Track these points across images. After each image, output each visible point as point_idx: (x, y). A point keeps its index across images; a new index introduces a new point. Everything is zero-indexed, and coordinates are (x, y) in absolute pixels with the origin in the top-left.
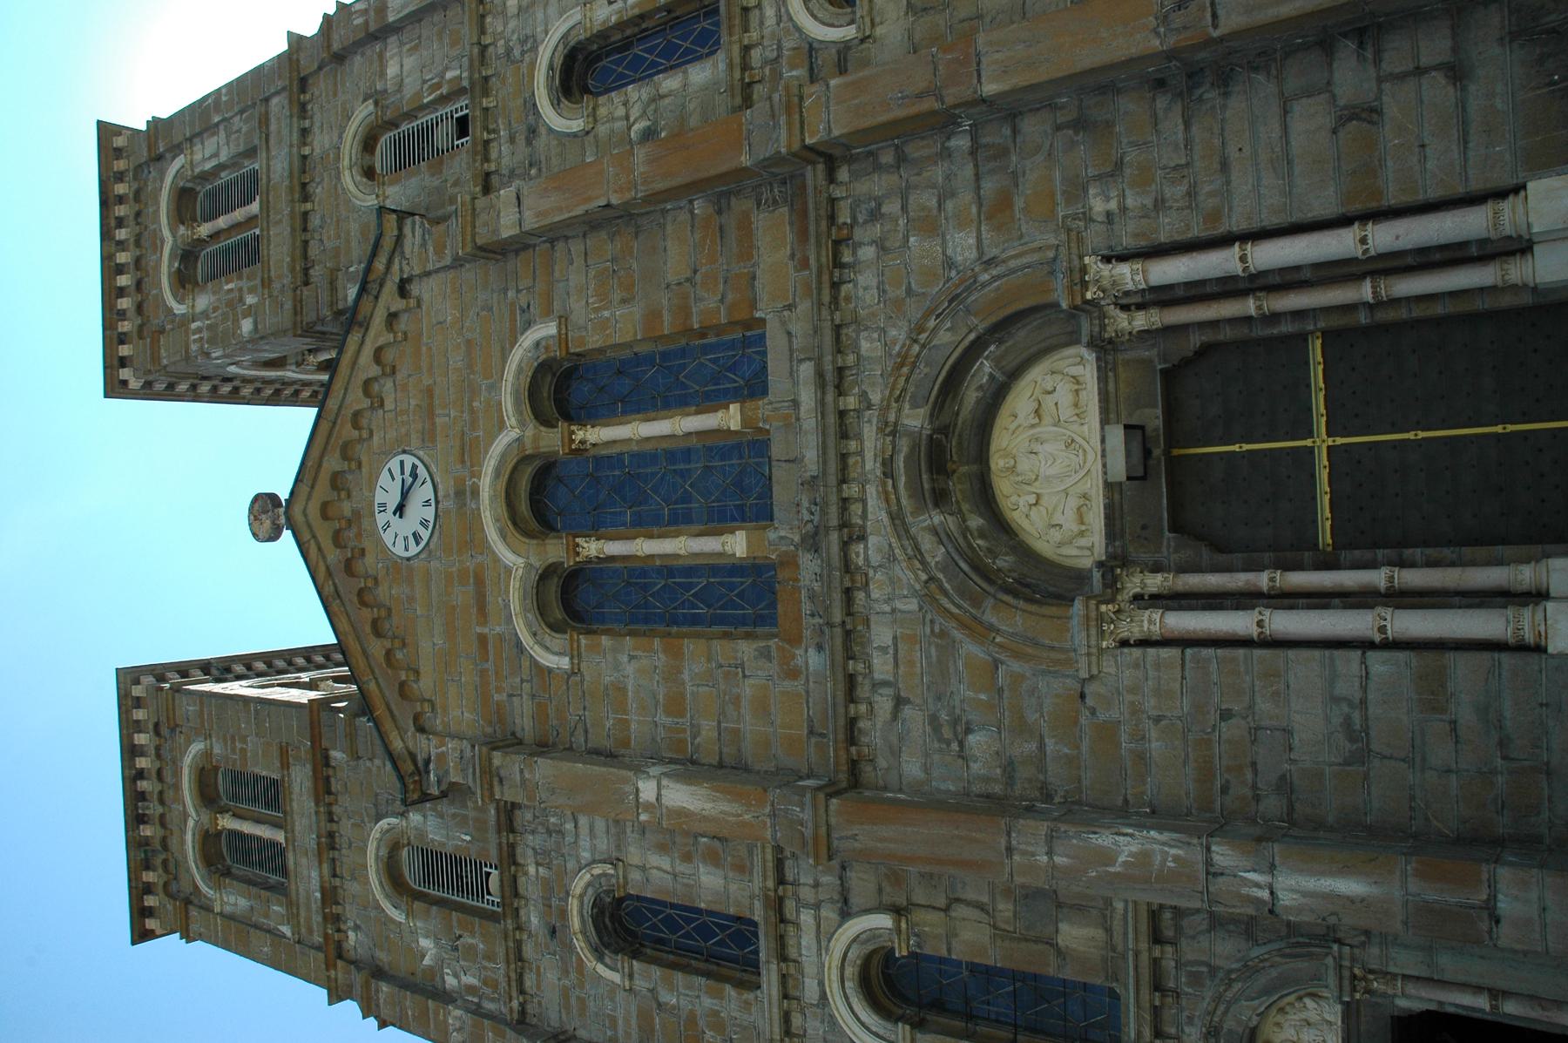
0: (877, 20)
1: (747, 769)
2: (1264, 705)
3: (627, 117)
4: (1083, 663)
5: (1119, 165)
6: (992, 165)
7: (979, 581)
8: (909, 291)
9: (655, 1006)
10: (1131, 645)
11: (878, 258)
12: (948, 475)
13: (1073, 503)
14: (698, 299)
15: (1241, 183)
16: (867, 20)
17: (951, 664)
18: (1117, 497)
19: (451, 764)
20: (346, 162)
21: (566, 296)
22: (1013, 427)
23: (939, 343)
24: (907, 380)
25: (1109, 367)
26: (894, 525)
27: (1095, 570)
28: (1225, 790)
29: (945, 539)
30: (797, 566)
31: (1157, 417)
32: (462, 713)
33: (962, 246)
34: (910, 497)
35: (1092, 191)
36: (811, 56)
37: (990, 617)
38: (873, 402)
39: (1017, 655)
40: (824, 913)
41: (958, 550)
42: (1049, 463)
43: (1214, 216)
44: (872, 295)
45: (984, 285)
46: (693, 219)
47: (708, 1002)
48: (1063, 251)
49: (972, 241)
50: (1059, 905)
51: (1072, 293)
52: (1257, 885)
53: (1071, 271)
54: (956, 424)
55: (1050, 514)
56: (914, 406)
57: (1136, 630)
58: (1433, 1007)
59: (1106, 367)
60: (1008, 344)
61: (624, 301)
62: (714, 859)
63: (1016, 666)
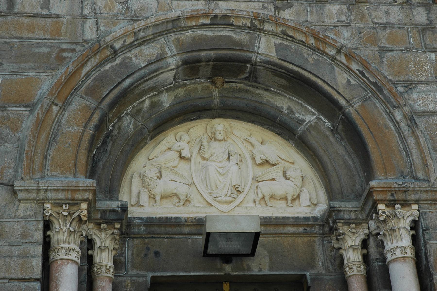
4: (31, 184)
8: (384, 50)
10: (45, 232)
11: (416, 25)
12: (211, 79)
13: (182, 190)
17: (32, 65)
18: (187, 230)
22: (253, 140)
23: (337, 73)
24: (302, 43)
25: (308, 229)
26: (167, 22)
27: (120, 203)
29: (154, 67)
31: (260, 270)
34: (193, 39)
38: (282, 12)
41: (143, 78)
42: (218, 169)
44: (381, 18)
45: (390, 115)
48: (425, 185)
51: (383, 191)
53: (405, 191)
54: (257, 88)
55: (172, 169)
56: (278, 48)
57: (61, 236)
59: (308, 225)
60: (331, 138)
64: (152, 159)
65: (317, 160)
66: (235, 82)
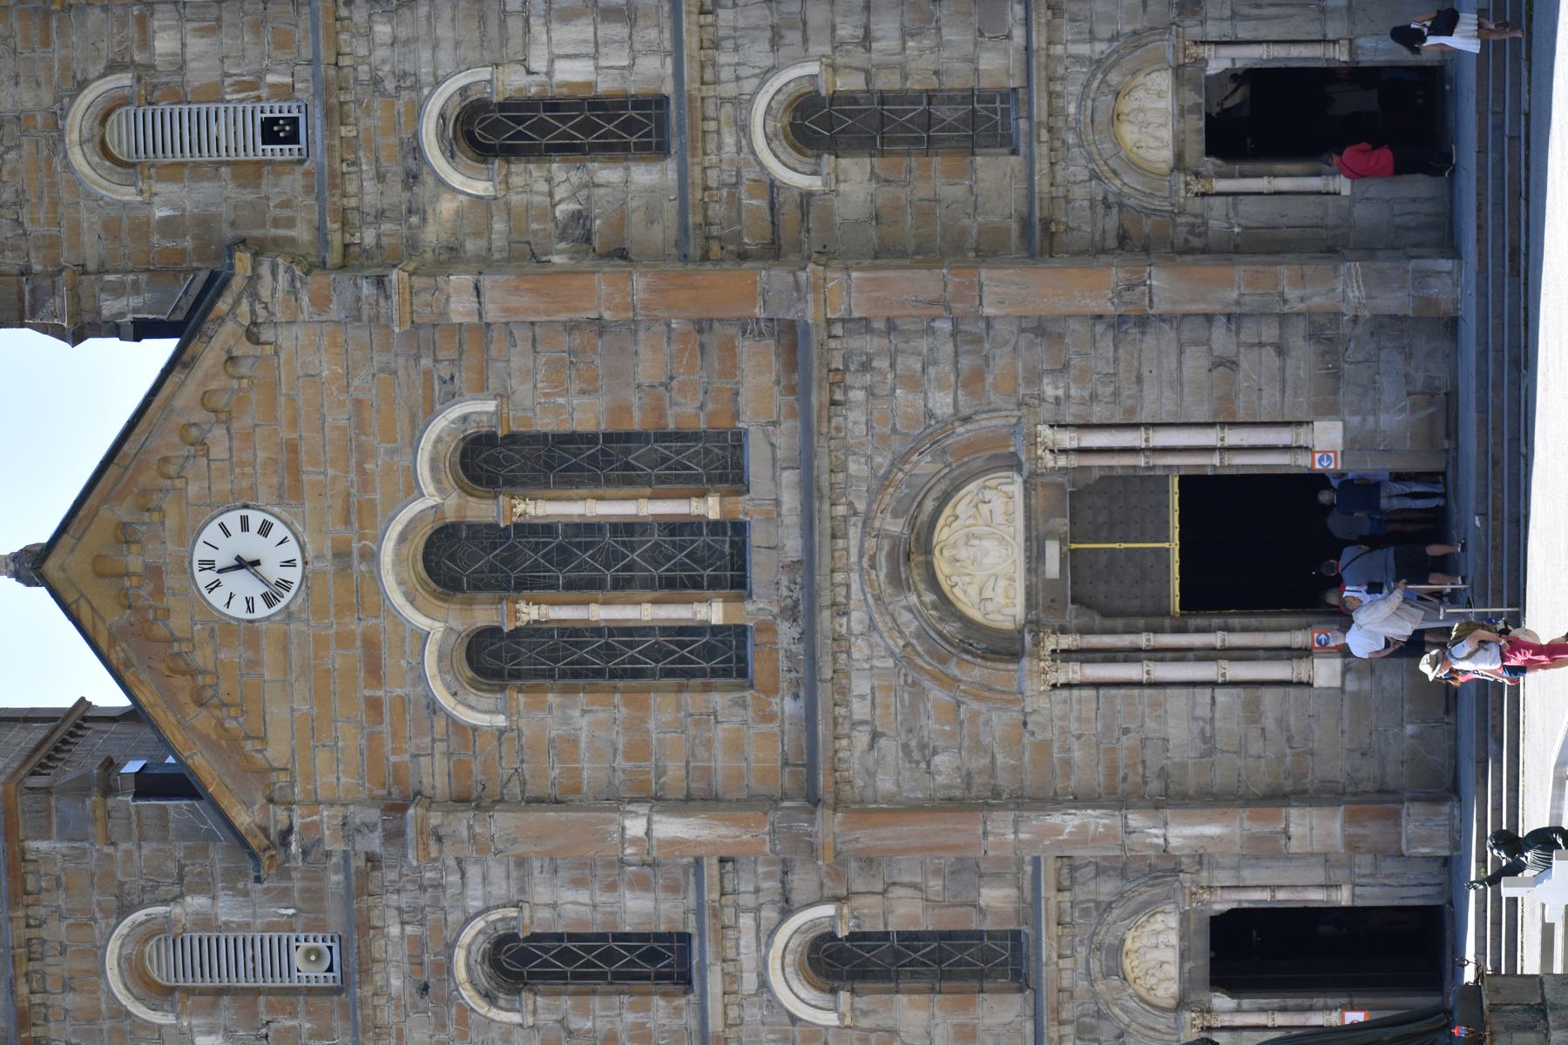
0: (842, 177)
1: (717, 799)
2: (1150, 724)
3: (551, 195)
5: (1066, 366)
6: (966, 348)
7: (947, 646)
8: (894, 431)
9: (563, 1034)
11: (867, 401)
14: (673, 404)
15: (1150, 392)
16: (833, 176)
17: (921, 705)
19: (327, 832)
20: (75, 136)
21: (506, 376)
28: (1125, 779)
30: (776, 632)
32: (338, 779)
33: (942, 403)
35: (1045, 380)
36: (772, 192)
37: (953, 669)
39: (977, 698)
40: (765, 913)
43: (1131, 411)
46: (669, 332)
47: (630, 1017)
49: (949, 400)
50: (981, 876)
52: (1156, 836)
58: (1235, 906)
61: (583, 392)
62: (642, 884)
63: (975, 705)
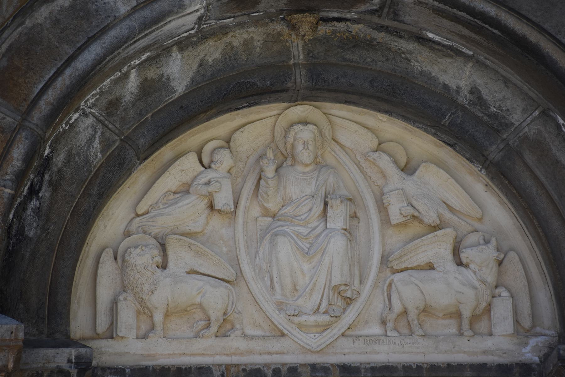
54: (397, 34)
64: (143, 215)
65: (536, 223)
66: (346, 20)
